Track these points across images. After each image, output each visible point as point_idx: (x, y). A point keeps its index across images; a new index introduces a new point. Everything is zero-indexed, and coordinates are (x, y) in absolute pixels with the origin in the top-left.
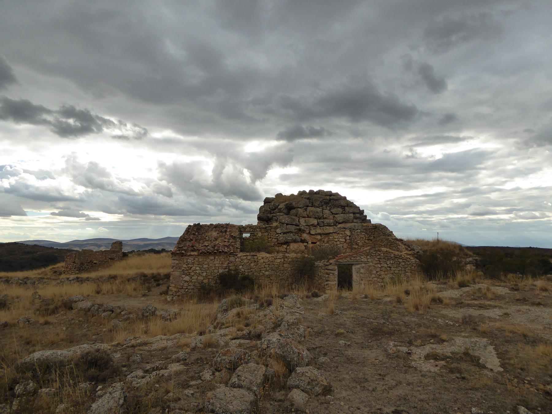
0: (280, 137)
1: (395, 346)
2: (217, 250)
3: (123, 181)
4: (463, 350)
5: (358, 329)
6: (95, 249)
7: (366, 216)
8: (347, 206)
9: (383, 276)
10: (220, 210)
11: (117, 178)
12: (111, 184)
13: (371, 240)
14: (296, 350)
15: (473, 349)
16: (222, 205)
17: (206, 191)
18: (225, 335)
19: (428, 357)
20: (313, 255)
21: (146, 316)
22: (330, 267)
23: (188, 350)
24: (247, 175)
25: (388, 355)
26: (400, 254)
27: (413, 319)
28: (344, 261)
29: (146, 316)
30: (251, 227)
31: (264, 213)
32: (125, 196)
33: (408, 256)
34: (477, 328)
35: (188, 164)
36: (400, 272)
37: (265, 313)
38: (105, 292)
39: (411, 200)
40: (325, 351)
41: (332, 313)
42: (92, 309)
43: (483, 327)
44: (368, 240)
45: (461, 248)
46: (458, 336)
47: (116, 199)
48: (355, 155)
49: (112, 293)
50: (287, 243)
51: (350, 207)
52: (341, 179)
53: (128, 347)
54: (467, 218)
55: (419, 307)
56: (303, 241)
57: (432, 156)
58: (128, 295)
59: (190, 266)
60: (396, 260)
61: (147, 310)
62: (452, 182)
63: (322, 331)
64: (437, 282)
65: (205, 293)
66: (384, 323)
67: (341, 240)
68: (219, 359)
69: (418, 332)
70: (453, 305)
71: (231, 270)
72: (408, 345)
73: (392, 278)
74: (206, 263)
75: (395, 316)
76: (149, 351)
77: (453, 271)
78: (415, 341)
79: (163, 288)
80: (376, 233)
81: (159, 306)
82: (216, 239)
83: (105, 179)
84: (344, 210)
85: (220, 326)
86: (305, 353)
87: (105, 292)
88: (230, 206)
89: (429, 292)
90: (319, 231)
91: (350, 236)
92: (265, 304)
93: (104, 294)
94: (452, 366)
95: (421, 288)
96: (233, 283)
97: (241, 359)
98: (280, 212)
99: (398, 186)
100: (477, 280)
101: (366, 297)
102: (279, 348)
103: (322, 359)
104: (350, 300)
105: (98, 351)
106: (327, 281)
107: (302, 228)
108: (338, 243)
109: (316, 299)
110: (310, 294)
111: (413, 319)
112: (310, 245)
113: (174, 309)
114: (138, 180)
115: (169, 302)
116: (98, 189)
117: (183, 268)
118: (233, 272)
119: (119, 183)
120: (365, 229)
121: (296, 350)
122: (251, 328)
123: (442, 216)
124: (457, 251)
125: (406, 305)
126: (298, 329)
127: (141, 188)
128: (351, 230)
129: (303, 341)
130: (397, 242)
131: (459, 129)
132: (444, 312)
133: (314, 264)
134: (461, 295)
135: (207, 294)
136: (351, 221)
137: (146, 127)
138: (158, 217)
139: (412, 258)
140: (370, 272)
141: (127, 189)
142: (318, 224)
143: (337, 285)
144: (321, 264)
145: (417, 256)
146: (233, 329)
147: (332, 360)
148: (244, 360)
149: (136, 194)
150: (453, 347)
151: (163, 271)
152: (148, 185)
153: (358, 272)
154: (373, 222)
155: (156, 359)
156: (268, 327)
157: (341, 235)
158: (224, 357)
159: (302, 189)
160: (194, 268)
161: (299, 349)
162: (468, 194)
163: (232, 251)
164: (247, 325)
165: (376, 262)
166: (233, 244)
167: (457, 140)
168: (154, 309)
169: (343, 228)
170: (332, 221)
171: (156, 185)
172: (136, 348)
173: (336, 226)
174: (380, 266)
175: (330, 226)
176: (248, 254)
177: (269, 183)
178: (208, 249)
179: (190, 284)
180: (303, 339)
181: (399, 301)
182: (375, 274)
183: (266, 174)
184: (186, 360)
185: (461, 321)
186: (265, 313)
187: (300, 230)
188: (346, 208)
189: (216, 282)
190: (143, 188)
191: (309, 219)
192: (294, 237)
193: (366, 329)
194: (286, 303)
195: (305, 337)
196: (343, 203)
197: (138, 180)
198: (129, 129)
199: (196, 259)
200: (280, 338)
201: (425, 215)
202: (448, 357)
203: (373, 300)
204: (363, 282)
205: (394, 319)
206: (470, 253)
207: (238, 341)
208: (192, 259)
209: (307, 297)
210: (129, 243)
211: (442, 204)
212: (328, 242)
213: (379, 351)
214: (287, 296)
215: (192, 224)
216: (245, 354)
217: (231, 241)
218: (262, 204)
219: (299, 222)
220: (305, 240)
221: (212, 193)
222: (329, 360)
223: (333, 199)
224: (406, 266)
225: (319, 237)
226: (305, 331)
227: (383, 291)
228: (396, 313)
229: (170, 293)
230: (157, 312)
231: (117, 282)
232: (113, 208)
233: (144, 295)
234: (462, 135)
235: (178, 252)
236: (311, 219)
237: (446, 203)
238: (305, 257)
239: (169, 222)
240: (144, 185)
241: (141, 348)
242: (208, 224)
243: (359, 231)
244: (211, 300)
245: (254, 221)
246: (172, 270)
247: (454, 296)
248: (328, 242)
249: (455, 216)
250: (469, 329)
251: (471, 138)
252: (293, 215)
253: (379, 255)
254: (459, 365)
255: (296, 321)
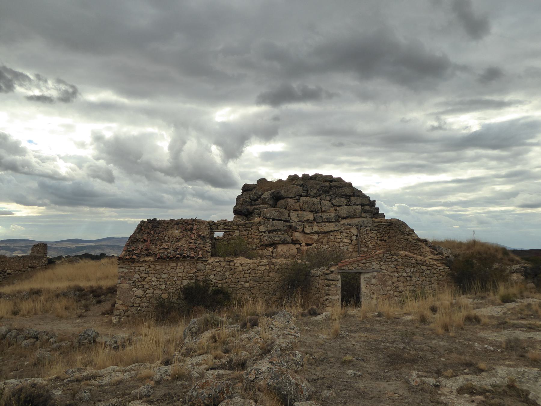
0: (263, 99)
1: (419, 376)
2: (181, 254)
3: (44, 160)
4: (507, 381)
5: (371, 355)
6: (8, 254)
7: (378, 209)
8: (354, 195)
9: (400, 289)
10: (180, 201)
11: (35, 157)
12: (27, 164)
13: (385, 241)
14: (293, 381)
15: (520, 382)
16: (183, 194)
17: (161, 175)
18: (199, 364)
19: (461, 391)
20: (308, 260)
21: (88, 342)
22: (331, 277)
23: (152, 383)
24: (216, 153)
25: (410, 388)
26: (423, 259)
27: (442, 343)
28: (349, 269)
29: (88, 342)
30: (225, 223)
31: (242, 204)
32: (47, 181)
33: (435, 262)
34: (526, 354)
35: (135, 138)
36: (424, 283)
37: (249, 335)
38: (25, 313)
39: (438, 187)
40: (329, 382)
41: (337, 335)
42: (8, 335)
43: (533, 353)
44: (381, 240)
45: (505, 251)
46: (501, 365)
47: (34, 184)
48: (363, 127)
49: (36, 314)
50: (273, 245)
51: (357, 196)
52: (343, 158)
53: (71, 381)
54: (513, 211)
55: (450, 328)
56: (294, 242)
57: (467, 128)
58: (58, 316)
59: (144, 276)
60: (419, 267)
61: (86, 335)
62: (494, 163)
63: (324, 359)
64: (473, 296)
65: (164, 312)
66: (404, 348)
67: (344, 240)
68: (195, 393)
69: (448, 359)
70: (493, 326)
71: (199, 281)
72: (435, 375)
73: (413, 291)
74: (165, 272)
75: (418, 338)
76: (99, 386)
77: (494, 282)
78: (444, 370)
79: (106, 306)
80: (392, 231)
81: (99, 329)
82: (178, 240)
83: (18, 158)
84: (350, 201)
85: (188, 353)
86: (304, 385)
87: (25, 313)
88: (194, 195)
89: (462, 310)
90: (315, 229)
91: (357, 236)
92: (248, 325)
93: (23, 315)
94: (493, 401)
95: (451, 303)
96: (202, 298)
97: (223, 393)
98: (264, 203)
99: (421, 168)
100: (525, 294)
101: (380, 315)
102: (272, 378)
103: (326, 393)
104: (360, 319)
105: (34, 385)
106: (327, 295)
107: (294, 224)
108: (341, 244)
109: (314, 318)
110: (307, 311)
111: (442, 343)
112: (305, 248)
113: (123, 334)
114: (66, 159)
115: (115, 325)
116: (10, 172)
117: (134, 279)
118: (201, 284)
119: (38, 163)
120: (377, 226)
121: (293, 381)
122: (232, 355)
123: (479, 208)
124: (500, 256)
125: (432, 325)
126: (294, 355)
127: (69, 170)
128: (358, 227)
129: (301, 371)
130: (420, 243)
131: (503, 90)
132: (482, 334)
133: (310, 272)
134: (504, 313)
135: (167, 313)
136: (358, 215)
137: (74, 84)
138: (94, 209)
139: (439, 265)
140: (384, 283)
141: (50, 172)
142: (315, 219)
143: (340, 300)
144: (319, 273)
145: (447, 262)
146: (208, 357)
147: (338, 395)
148: (227, 394)
149: (64, 179)
150: (495, 379)
151: (105, 284)
152: (80, 167)
153: (367, 284)
154: (389, 216)
155: (110, 396)
156: (254, 354)
157: (345, 234)
158: (201, 391)
159: (293, 172)
160: (149, 278)
161: (297, 380)
162: (515, 178)
163: (200, 256)
164: (226, 351)
165: (392, 270)
166: (201, 246)
167: (501, 105)
168: (94, 334)
169: (347, 225)
170: (333, 215)
171: (91, 166)
172: (82, 383)
173: (339, 222)
174: (396, 275)
175: (330, 222)
176: (222, 259)
177: (246, 163)
178: (168, 253)
179: (144, 300)
180: (300, 368)
181: (423, 320)
182: (390, 286)
183: (242, 152)
184: (149, 396)
185: (504, 345)
186: (249, 335)
187: (290, 227)
188: (352, 198)
189: (179, 296)
190: (73, 170)
191: (302, 212)
192: (283, 237)
193: (381, 356)
194: (275, 323)
195: (302, 366)
196: (347, 191)
197: (66, 159)
198: (51, 89)
199: (152, 266)
200: (272, 367)
201: (457, 208)
202: (488, 391)
203: (389, 318)
204: (374, 296)
205: (417, 342)
206: (517, 258)
207: (216, 372)
208: (147, 266)
209: (303, 315)
210: (54, 246)
211: (480, 193)
212: (327, 243)
213: (398, 383)
214: (277, 313)
215: (146, 220)
216: (228, 386)
217: (199, 242)
218: (240, 192)
219: (289, 216)
220: (297, 240)
221: (169, 178)
222: (334, 394)
223: (335, 186)
224: (432, 275)
225: (316, 237)
226: (302, 358)
227: (402, 308)
228: (420, 335)
229: (116, 312)
230: (99, 339)
231: (42, 298)
232: (31, 198)
233: (80, 316)
234: (507, 98)
235: (127, 257)
236: (305, 213)
237: (485, 192)
238: (297, 264)
239: (110, 216)
240: (73, 166)
241: (89, 382)
242: (168, 219)
243: (369, 228)
244: (174, 322)
245: (230, 216)
246: (119, 281)
247: (495, 314)
248: (327, 243)
249: (498, 209)
250: (514, 356)
251: (520, 102)
252: (281, 207)
253: (396, 260)
254: (501, 401)
255: (290, 345)
